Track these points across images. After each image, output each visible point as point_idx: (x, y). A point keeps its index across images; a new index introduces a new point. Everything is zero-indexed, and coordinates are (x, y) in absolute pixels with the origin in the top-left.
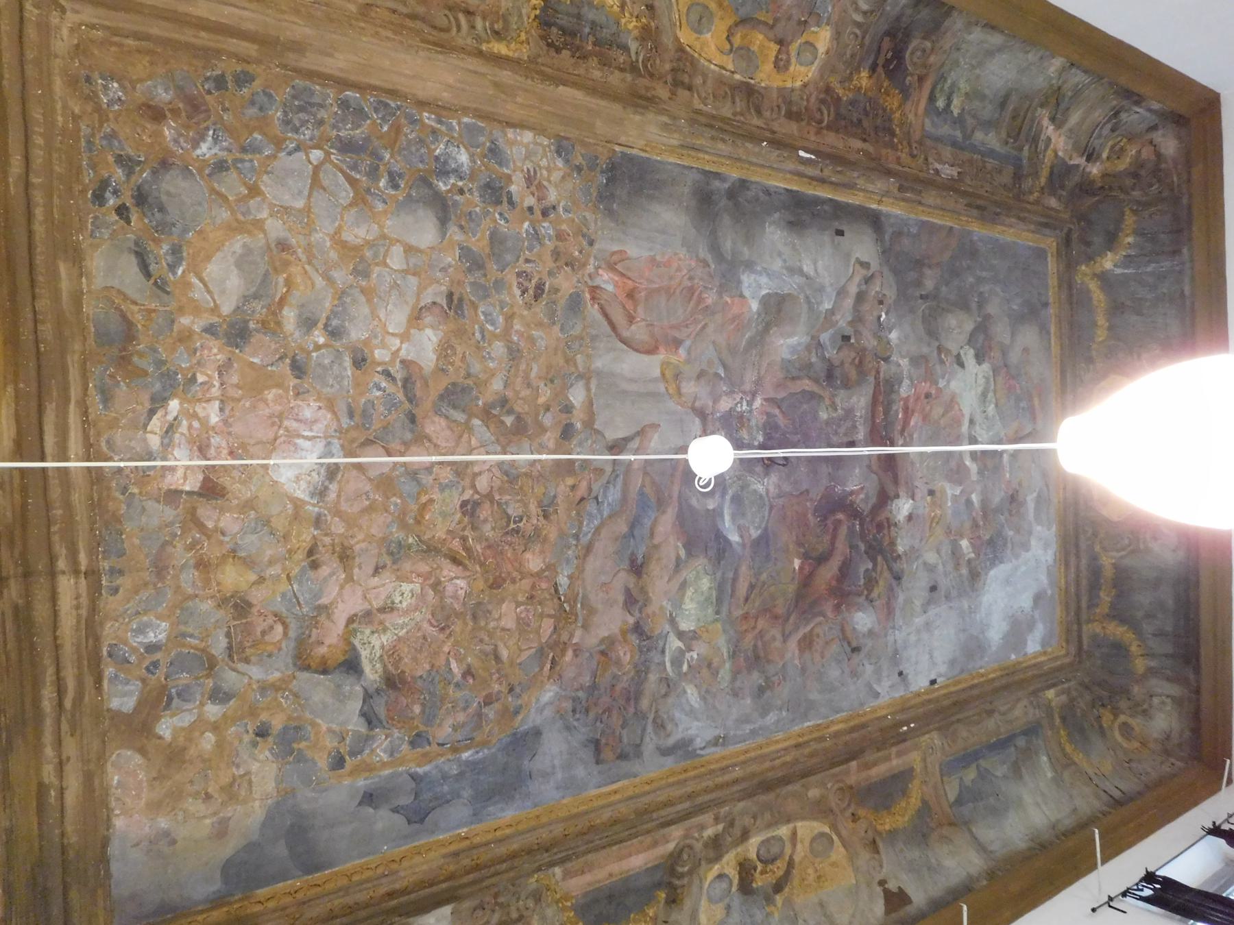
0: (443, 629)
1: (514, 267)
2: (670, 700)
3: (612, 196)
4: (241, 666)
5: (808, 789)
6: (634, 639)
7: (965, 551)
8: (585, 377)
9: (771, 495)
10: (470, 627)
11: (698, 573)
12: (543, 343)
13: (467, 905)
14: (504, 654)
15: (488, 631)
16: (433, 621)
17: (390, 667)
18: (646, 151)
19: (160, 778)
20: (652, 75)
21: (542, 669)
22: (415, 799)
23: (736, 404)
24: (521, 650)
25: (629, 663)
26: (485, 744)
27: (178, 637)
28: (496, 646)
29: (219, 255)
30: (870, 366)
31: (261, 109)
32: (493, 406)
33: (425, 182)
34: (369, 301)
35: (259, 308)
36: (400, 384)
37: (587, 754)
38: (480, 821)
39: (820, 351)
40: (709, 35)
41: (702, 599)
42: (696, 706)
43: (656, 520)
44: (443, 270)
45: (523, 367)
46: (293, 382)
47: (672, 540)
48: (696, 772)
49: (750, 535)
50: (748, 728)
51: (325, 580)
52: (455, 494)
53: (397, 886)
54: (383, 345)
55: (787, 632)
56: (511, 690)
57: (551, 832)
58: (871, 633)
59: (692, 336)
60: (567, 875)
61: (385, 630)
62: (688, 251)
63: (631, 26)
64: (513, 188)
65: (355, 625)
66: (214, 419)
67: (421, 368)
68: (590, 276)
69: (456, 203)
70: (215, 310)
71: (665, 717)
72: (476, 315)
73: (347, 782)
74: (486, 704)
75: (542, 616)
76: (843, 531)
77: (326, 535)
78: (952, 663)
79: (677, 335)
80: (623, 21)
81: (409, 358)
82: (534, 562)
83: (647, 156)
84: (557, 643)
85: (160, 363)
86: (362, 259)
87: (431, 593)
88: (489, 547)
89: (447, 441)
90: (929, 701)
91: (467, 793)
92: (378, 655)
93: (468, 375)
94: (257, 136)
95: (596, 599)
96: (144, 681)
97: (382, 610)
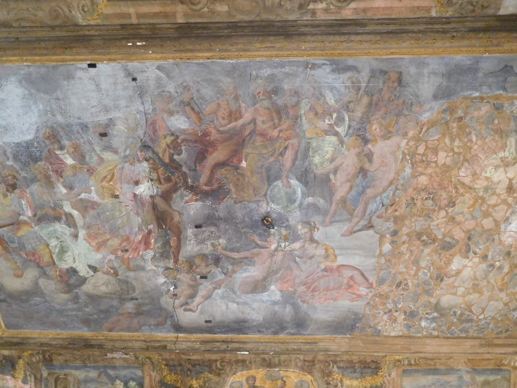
2: (347, 99)
3: (354, 320)
5: (228, 12)
6: (368, 136)
7: (67, 156)
9: (265, 202)
11: (322, 166)
12: (401, 266)
13: (490, 12)
26: (466, 98)
32: (431, 243)
33: (442, 315)
37: (406, 78)
40: (296, 381)
42: (327, 92)
43: (348, 194)
47: (338, 184)
50: (287, 69)
54: (474, 263)
58: (171, 113)
61: (501, 158)
63: (337, 375)
67: (461, 256)
76: (203, 179)
78: (69, 77)
80: (341, 376)
82: (423, 180)
84: (418, 141)
87: (478, 171)
88: (445, 188)
93: (440, 254)
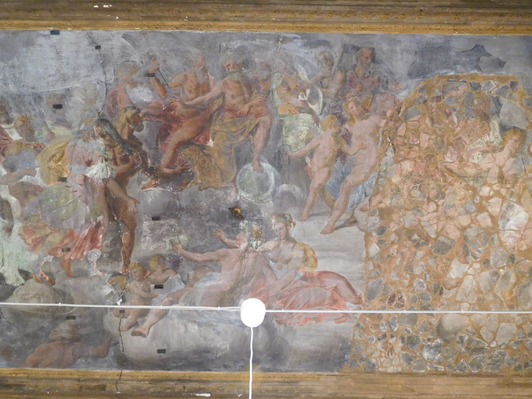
0: (460, 139)
2: (320, 74)
3: (342, 349)
6: (346, 116)
7: (14, 130)
8: (368, 259)
9: (234, 189)
10: (446, 137)
11: (296, 147)
12: (392, 274)
14: (428, 121)
16: (464, 143)
17: (487, 125)
18: (318, 375)
21: (406, 109)
22: (479, 58)
23: (261, 245)
26: (441, 77)
28: (432, 126)
31: (513, 358)
32: (423, 244)
33: (447, 342)
34: (479, 288)
36: (470, 254)
37: (379, 55)
39: (185, 279)
41: (293, 131)
42: (300, 66)
45: (405, 263)
46: (515, 253)
47: (315, 169)
48: (303, 25)
49: (253, 165)
53: (497, 18)
54: (475, 270)
55: (221, 99)
56: (425, 101)
57: (412, 19)
61: (487, 143)
62: (292, 328)
64: (401, 345)
65: (500, 147)
67: (459, 260)
69: (432, 334)
71: (324, 65)
72: (427, 286)
73: (510, 75)
75: (405, 137)
76: (165, 160)
77: (508, 188)
78: (29, 43)
79: (304, 283)
81: (464, 265)
84: (396, 121)
90: (64, 19)
91: (453, 53)
92: (491, 131)
93: (435, 258)
94: (515, 348)
95: (369, 141)
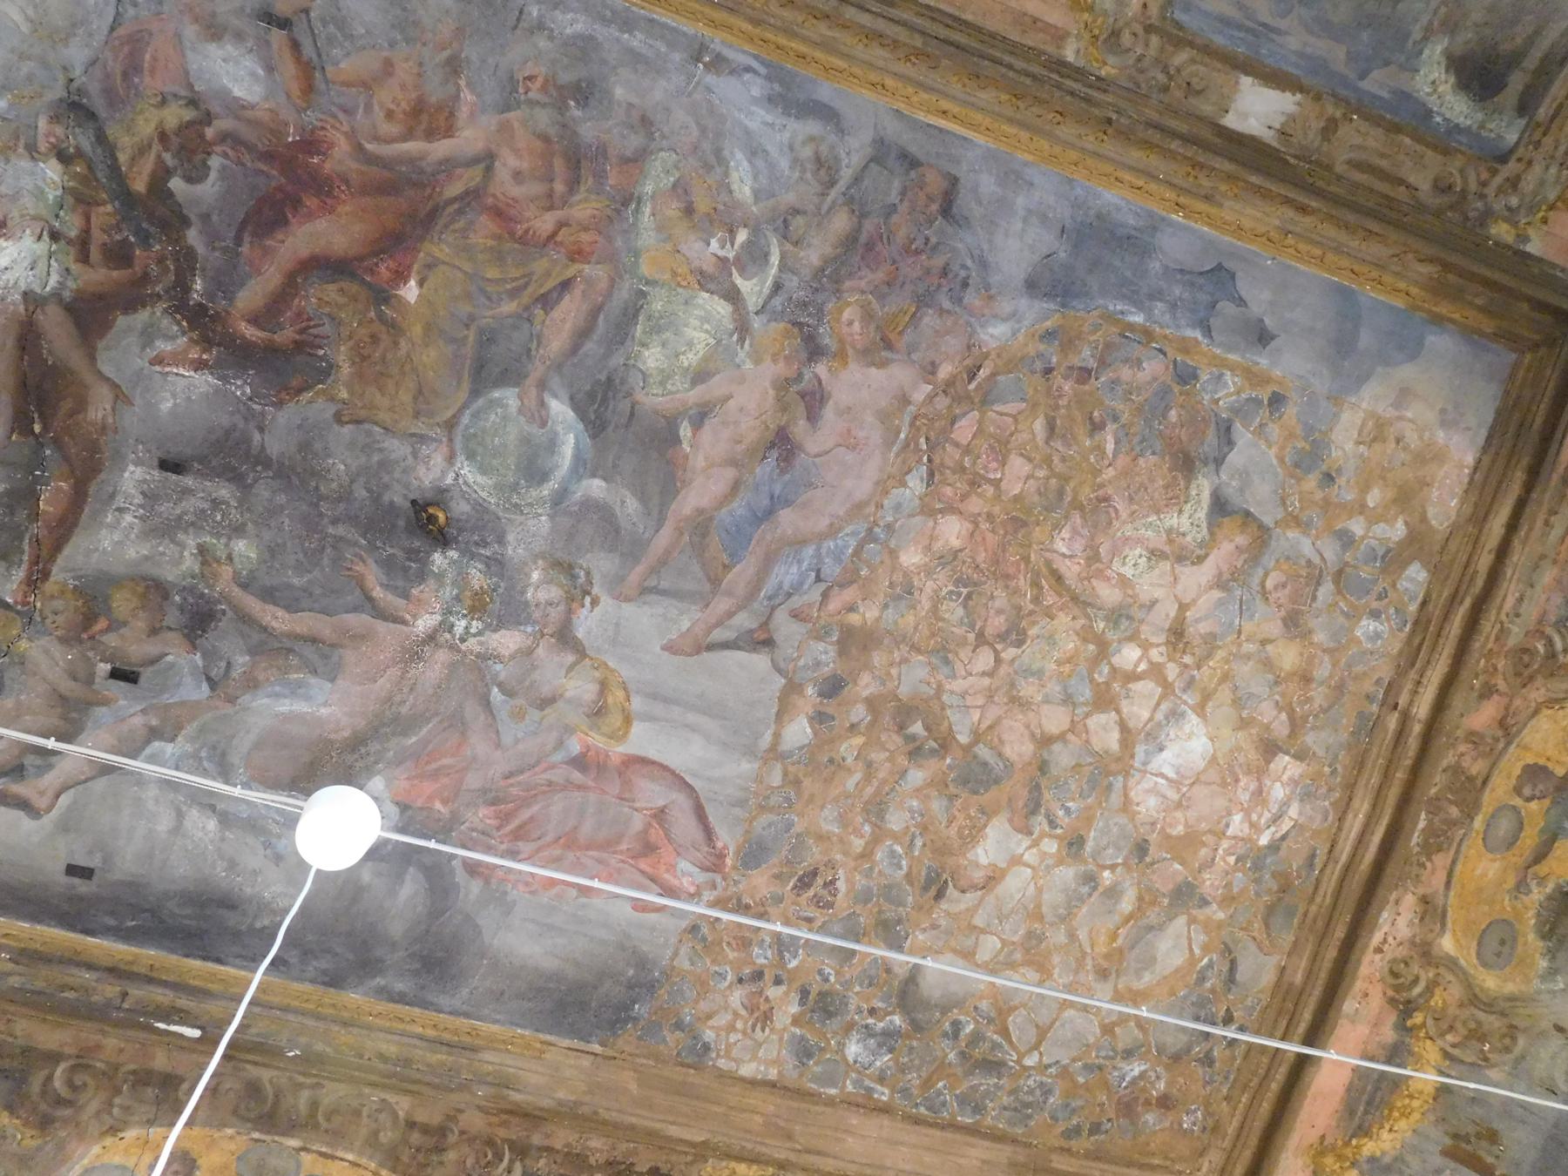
1: (834, 915)
4: (1317, 560)
8: (775, 753)
9: (445, 449)
11: (662, 383)
12: (826, 812)
13: (1206, 108)
14: (1039, 426)
15: (1049, 466)
19: (1425, 484)
20: (490, 1143)
21: (993, 375)
23: (479, 633)
24: (1014, 417)
25: (849, 304)
26: (1110, 318)
27: (1353, 616)
29: (1166, 973)
30: (58, 604)
31: (1067, 1105)
33: (917, 1027)
34: (1039, 906)
35: (1152, 916)
37: (965, 202)
38: (1151, 215)
42: (739, 155)
44: (934, 927)
45: (869, 790)
47: (699, 462)
48: (782, 41)
49: (520, 398)
50: (637, 41)
51: (1206, 618)
52: (1026, 659)
54: (1043, 856)
56: (1048, 371)
57: (1080, 136)
59: (544, 765)
60: (1060, 37)
61: (1169, 531)
64: (794, 1009)
65: (1199, 552)
66: (1237, 818)
67: (1010, 821)
68: (714, 887)
70: (1192, 921)
71: (809, 175)
72: (910, 868)
73: (1277, 373)
74: (1088, 371)
75: (967, 450)
76: (251, 295)
83: (541, 1036)
84: (958, 399)
85: (1257, 881)
86: (1027, 951)
89: (1011, 728)
91: (1155, 266)
93: (952, 798)
94: (1081, 1080)
95: (871, 431)
96: (1394, 586)
97: (1162, 556)
